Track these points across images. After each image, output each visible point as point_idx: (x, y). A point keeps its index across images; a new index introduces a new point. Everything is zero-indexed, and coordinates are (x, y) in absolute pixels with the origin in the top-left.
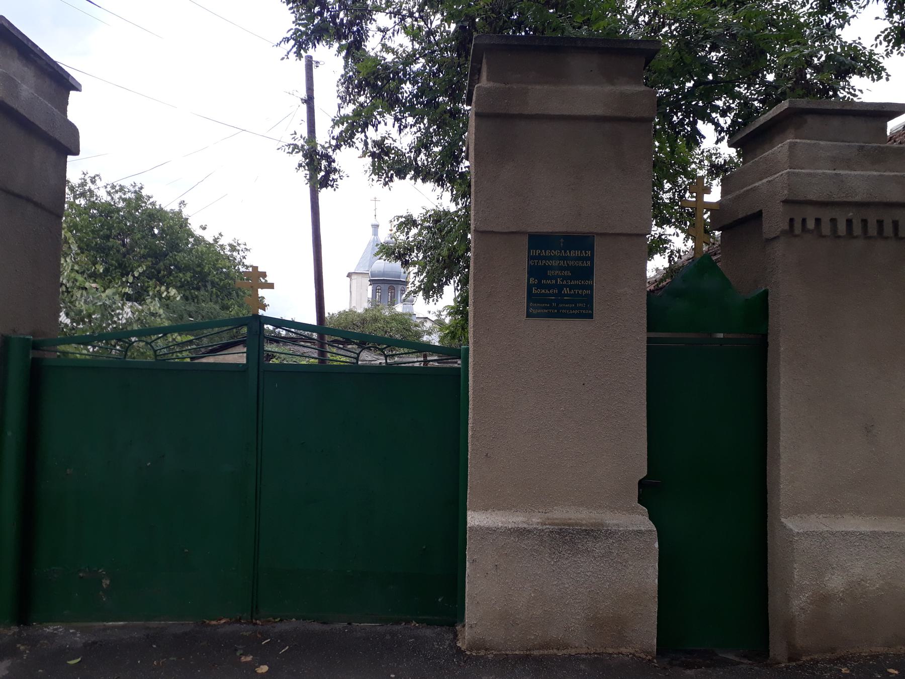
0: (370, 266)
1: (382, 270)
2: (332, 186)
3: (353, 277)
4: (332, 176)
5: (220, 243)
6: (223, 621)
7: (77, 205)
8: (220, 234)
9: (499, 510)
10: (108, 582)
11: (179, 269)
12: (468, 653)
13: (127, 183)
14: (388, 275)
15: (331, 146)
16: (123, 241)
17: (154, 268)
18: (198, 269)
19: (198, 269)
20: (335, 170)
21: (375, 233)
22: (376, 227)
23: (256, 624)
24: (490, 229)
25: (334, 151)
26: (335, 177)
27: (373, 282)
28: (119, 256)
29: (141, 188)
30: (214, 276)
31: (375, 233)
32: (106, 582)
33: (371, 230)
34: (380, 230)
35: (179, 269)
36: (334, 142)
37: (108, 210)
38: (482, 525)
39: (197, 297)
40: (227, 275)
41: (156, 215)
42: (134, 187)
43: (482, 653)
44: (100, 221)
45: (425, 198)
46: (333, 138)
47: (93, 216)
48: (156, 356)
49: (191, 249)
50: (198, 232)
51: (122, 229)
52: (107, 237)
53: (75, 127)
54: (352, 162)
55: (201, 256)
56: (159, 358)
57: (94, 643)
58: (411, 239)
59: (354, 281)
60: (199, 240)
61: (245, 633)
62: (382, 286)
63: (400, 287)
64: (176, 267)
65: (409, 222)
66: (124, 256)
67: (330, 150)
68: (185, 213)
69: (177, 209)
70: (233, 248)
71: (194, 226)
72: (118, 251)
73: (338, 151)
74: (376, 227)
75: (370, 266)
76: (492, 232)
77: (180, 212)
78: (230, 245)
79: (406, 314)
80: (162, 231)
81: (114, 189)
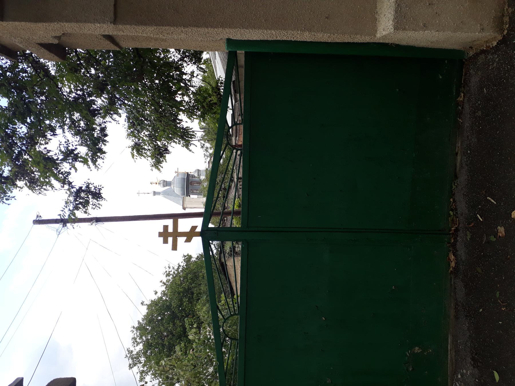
0: (177, 196)
1: (180, 189)
2: (100, 189)
3: (185, 206)
4: (92, 189)
5: (165, 281)
6: (452, 257)
7: (145, 362)
8: (161, 282)
9: (376, 8)
10: (417, 348)
11: (181, 305)
12: (505, 32)
13: (132, 335)
14: (183, 185)
15: (69, 190)
16: (166, 336)
17: (181, 318)
18: (182, 294)
19: (182, 294)
20: (88, 187)
21: (159, 193)
22: (155, 193)
23: (457, 230)
24: (112, 8)
25: (73, 187)
26: (93, 188)
27: (188, 195)
28: (174, 338)
29: (134, 327)
30: (185, 285)
31: (159, 193)
32: (417, 350)
33: (157, 196)
34: (156, 191)
35: (181, 305)
36: (66, 187)
37: (148, 345)
38: (392, 18)
39: (197, 295)
40: (185, 278)
41: (149, 319)
42: (133, 331)
43: (506, 19)
44: (154, 349)
45: (117, 129)
46: (63, 187)
47: (151, 353)
48: (235, 314)
49: (169, 298)
50: (159, 295)
51: (158, 337)
52: (163, 346)
53: (52, 382)
54: (81, 175)
55: (173, 292)
56: (237, 313)
57: (473, 359)
58: (150, 148)
59: (188, 206)
60: (164, 293)
61: (469, 237)
62: (190, 189)
63: (190, 178)
64: (180, 306)
65: (138, 148)
66: (173, 335)
67: (72, 190)
68: (149, 303)
69: (146, 307)
70: (168, 275)
71: (155, 297)
72: (171, 339)
73: (73, 184)
74: (155, 193)
75: (177, 196)
76: (115, 5)
77: (148, 306)
78: (166, 277)
79: (206, 172)
80: (159, 315)
81: (135, 341)
